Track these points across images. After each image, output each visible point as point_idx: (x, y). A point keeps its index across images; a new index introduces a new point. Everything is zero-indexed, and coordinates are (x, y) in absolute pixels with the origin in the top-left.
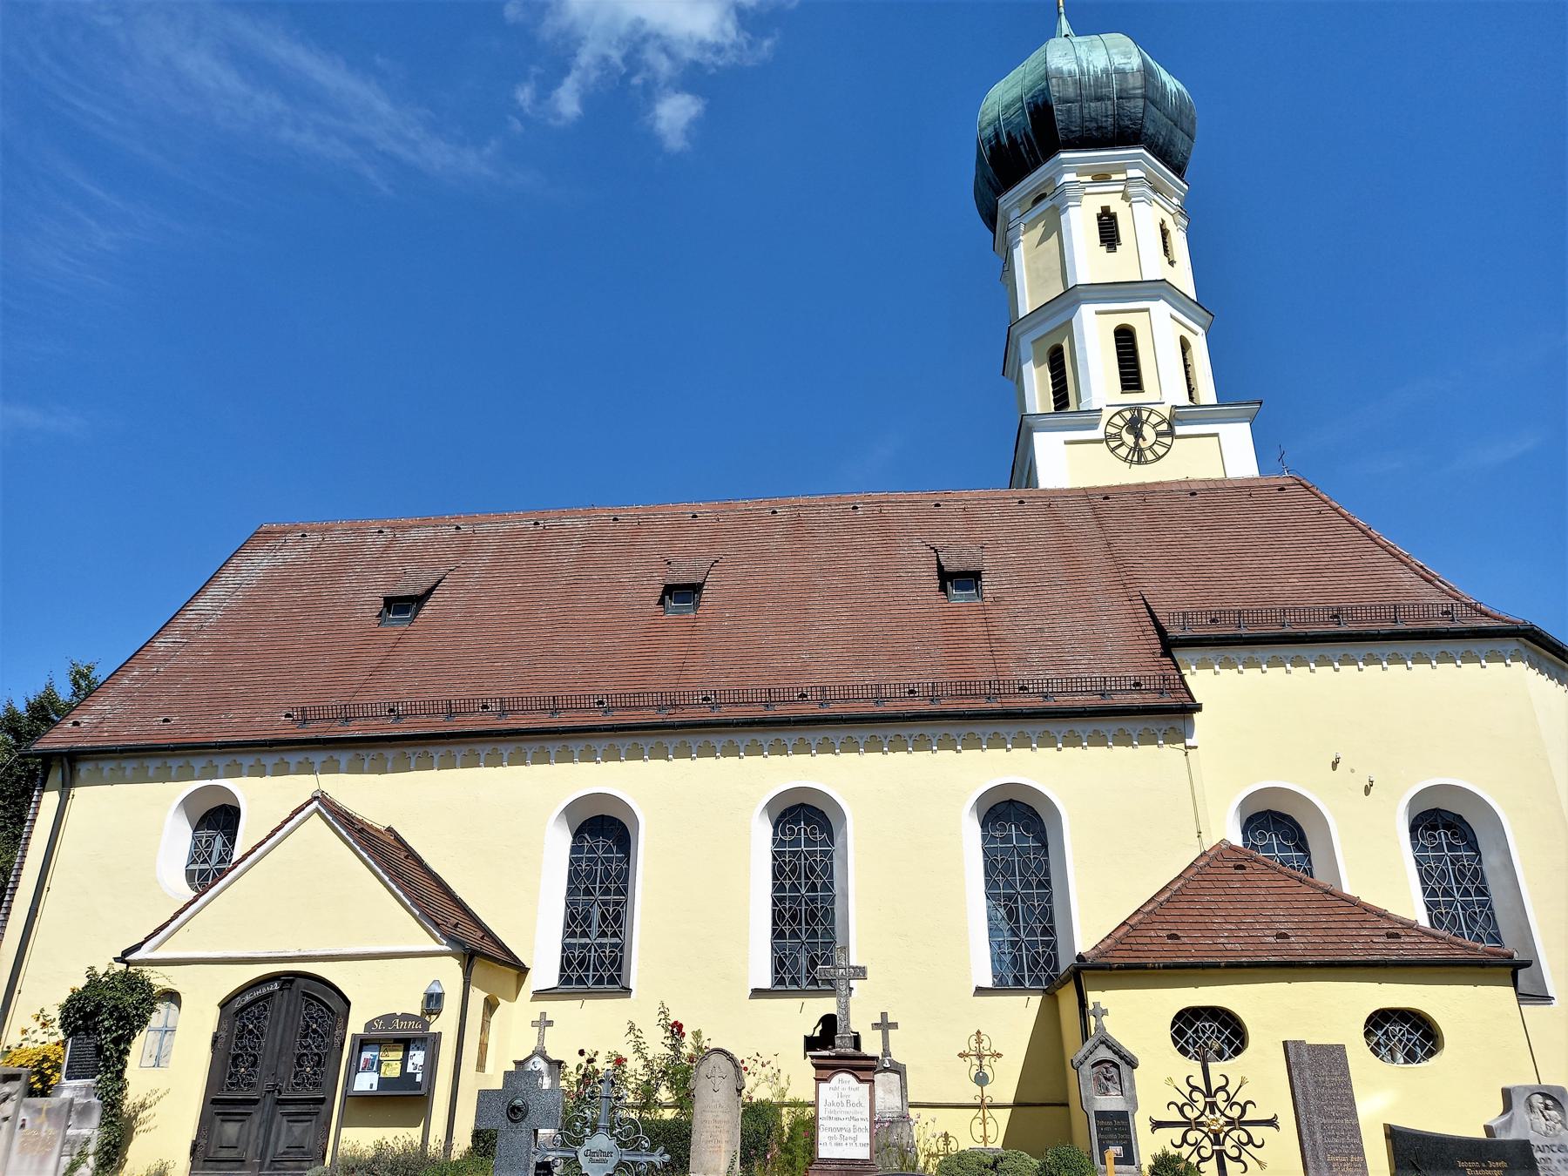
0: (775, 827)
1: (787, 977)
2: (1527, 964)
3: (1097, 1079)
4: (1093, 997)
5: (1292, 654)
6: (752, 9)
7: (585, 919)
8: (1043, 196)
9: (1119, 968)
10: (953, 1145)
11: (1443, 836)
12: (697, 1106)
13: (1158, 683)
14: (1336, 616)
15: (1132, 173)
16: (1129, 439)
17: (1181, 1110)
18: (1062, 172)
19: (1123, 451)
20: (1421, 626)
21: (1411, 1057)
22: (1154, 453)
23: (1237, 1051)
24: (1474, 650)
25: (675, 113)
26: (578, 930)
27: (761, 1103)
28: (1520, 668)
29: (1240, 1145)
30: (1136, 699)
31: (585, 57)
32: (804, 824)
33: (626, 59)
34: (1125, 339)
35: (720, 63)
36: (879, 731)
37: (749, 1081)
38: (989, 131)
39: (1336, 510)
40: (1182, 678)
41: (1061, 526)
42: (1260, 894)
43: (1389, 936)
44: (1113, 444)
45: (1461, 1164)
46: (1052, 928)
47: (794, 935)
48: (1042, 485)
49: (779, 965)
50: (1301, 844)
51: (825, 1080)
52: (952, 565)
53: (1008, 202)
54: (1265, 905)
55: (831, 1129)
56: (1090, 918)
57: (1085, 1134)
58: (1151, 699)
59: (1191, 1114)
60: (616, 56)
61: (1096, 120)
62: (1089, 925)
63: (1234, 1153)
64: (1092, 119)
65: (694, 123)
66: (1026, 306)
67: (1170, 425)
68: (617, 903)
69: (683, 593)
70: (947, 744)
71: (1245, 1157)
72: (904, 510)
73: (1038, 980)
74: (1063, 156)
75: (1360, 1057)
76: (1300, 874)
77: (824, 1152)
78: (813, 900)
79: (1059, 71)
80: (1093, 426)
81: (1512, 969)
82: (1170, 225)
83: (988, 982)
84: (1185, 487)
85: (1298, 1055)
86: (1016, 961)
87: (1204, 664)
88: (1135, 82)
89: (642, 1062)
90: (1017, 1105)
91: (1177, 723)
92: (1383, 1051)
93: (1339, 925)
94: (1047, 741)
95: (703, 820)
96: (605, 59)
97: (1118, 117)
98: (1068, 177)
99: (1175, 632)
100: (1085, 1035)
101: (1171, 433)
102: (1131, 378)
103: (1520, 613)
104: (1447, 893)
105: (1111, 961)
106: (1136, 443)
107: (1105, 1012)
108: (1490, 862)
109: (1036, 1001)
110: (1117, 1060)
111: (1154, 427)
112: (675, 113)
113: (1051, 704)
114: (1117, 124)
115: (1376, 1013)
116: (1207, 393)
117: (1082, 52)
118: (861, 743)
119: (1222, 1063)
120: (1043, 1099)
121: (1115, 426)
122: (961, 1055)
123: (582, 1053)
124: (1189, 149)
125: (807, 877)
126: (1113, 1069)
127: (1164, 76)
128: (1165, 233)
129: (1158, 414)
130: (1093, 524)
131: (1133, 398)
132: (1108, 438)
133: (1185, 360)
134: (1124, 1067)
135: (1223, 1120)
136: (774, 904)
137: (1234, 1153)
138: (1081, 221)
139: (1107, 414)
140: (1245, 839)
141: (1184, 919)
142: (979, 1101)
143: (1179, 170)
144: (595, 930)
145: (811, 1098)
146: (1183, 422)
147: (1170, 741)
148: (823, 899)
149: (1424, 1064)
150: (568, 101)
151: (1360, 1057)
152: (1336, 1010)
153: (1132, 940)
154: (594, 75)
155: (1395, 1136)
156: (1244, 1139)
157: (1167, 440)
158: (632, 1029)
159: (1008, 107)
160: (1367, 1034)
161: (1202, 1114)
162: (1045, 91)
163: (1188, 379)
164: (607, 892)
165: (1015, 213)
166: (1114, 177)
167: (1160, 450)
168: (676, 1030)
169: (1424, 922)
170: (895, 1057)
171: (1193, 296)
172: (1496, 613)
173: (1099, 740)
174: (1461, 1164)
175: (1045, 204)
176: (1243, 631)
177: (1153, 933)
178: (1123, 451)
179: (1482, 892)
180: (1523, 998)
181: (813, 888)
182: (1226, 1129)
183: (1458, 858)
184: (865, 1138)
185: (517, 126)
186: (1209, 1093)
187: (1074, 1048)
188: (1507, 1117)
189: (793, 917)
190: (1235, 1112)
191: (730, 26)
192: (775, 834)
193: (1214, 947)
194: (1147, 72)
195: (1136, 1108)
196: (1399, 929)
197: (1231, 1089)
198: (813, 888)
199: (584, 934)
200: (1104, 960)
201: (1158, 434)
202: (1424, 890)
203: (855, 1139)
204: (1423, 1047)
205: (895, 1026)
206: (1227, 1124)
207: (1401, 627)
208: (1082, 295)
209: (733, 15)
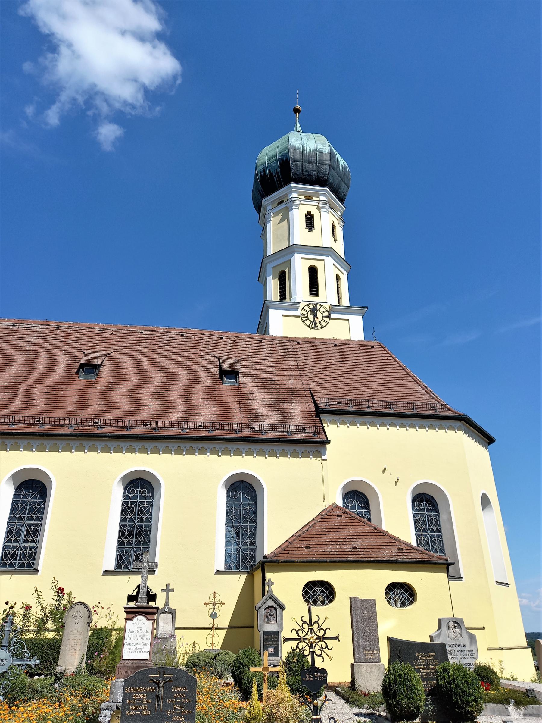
0: (125, 489)
1: (123, 565)
2: (453, 564)
3: (266, 616)
4: (269, 576)
5: (370, 421)
6: (152, 91)
7: (17, 533)
8: (282, 202)
9: (282, 562)
10: (197, 648)
11: (425, 505)
12: (66, 632)
13: (312, 430)
14: (390, 405)
15: (322, 198)
16: (311, 317)
17: (297, 633)
18: (291, 192)
19: (308, 322)
20: (423, 412)
21: (403, 604)
22: (321, 324)
23: (330, 601)
24: (443, 424)
25: (108, 132)
26: (13, 539)
27: (102, 629)
28: (461, 433)
29: (322, 649)
30: (302, 436)
31: (64, 97)
32: (140, 489)
33: (86, 102)
34: (313, 271)
35: (133, 113)
36: (182, 444)
37: (95, 617)
38: (261, 168)
39: (394, 358)
40: (323, 428)
41: (277, 354)
42: (347, 531)
43: (399, 549)
44: (304, 319)
45: (417, 654)
46: (255, 542)
47: (129, 543)
48: (271, 334)
49: (120, 558)
50: (367, 506)
51: (130, 619)
52: (226, 367)
53: (267, 201)
54: (349, 534)
55: (130, 645)
56: (273, 536)
57: (259, 640)
58: (309, 437)
59: (302, 634)
60: (81, 100)
61: (308, 172)
62: (271, 542)
63: (319, 653)
64: (306, 171)
65: (118, 139)
66: (271, 250)
67: (329, 313)
68: (36, 525)
69: (90, 368)
70: (215, 452)
71: (324, 655)
72: (206, 339)
73: (246, 567)
74: (292, 185)
75: (382, 604)
76: (365, 520)
77: (125, 656)
78: (141, 526)
79: (294, 147)
80: (296, 309)
81: (446, 565)
82: (336, 224)
83: (222, 568)
84: (332, 342)
85: (355, 603)
86: (237, 558)
87: (333, 422)
88: (326, 158)
89: (40, 608)
90: (230, 627)
91: (319, 448)
92: (392, 601)
93: (379, 544)
94: (261, 453)
95: (86, 485)
96: (75, 100)
97: (318, 172)
98: (294, 195)
99: (322, 407)
100: (264, 594)
101: (329, 317)
102: (314, 290)
103: (463, 411)
104: (425, 530)
105: (279, 559)
106: (314, 319)
107: (273, 583)
108: (443, 517)
109: (244, 577)
110: (276, 606)
111: (322, 313)
112: (108, 132)
113: (264, 436)
114: (317, 175)
115: (390, 584)
116: (346, 301)
117: (305, 140)
118: (173, 449)
119: (323, 607)
120: (242, 625)
121: (305, 310)
122: (205, 604)
123: (7, 603)
124: (347, 192)
125: (139, 515)
126: (274, 611)
127: (339, 157)
128: (334, 227)
129: (324, 308)
130: (292, 354)
131: (314, 299)
132: (302, 316)
133: (338, 285)
134: (279, 610)
135: (315, 637)
136: (120, 528)
137: (319, 653)
138: (298, 217)
139: (302, 304)
140: (344, 503)
141: (313, 539)
142: (211, 626)
143: (342, 200)
144: (22, 538)
145: (123, 626)
146: (335, 312)
147: (316, 456)
148: (146, 526)
149: (408, 607)
150: (53, 117)
151: (382, 604)
152: (371, 583)
153: (289, 549)
154: (68, 106)
155: (390, 640)
156: (324, 646)
157: (327, 320)
158: (36, 591)
159: (270, 158)
160: (386, 594)
161: (307, 634)
162: (287, 154)
163: (338, 294)
164: (31, 519)
165: (269, 208)
166: (314, 199)
167: (324, 324)
168: (60, 591)
169: (414, 543)
170: (170, 606)
171: (344, 257)
172: (453, 409)
173: (284, 454)
174: (417, 654)
175: (283, 206)
176: (351, 409)
177: (299, 546)
178: (308, 322)
179: (439, 530)
180: (451, 577)
181: (141, 520)
182: (316, 641)
183: (430, 515)
184: (147, 648)
185: (25, 125)
186: (310, 624)
187: (259, 600)
188: (439, 632)
189: (129, 535)
190: (321, 633)
191: (140, 96)
192: (125, 492)
193: (325, 553)
194: (332, 155)
195: (282, 629)
196: (403, 546)
197: (320, 622)
198: (141, 520)
199: (16, 541)
200: (276, 558)
201: (324, 317)
202: (416, 529)
203: (142, 649)
204: (408, 599)
205: (173, 590)
206: (317, 639)
207: (415, 412)
208: (296, 249)
209: (142, 90)
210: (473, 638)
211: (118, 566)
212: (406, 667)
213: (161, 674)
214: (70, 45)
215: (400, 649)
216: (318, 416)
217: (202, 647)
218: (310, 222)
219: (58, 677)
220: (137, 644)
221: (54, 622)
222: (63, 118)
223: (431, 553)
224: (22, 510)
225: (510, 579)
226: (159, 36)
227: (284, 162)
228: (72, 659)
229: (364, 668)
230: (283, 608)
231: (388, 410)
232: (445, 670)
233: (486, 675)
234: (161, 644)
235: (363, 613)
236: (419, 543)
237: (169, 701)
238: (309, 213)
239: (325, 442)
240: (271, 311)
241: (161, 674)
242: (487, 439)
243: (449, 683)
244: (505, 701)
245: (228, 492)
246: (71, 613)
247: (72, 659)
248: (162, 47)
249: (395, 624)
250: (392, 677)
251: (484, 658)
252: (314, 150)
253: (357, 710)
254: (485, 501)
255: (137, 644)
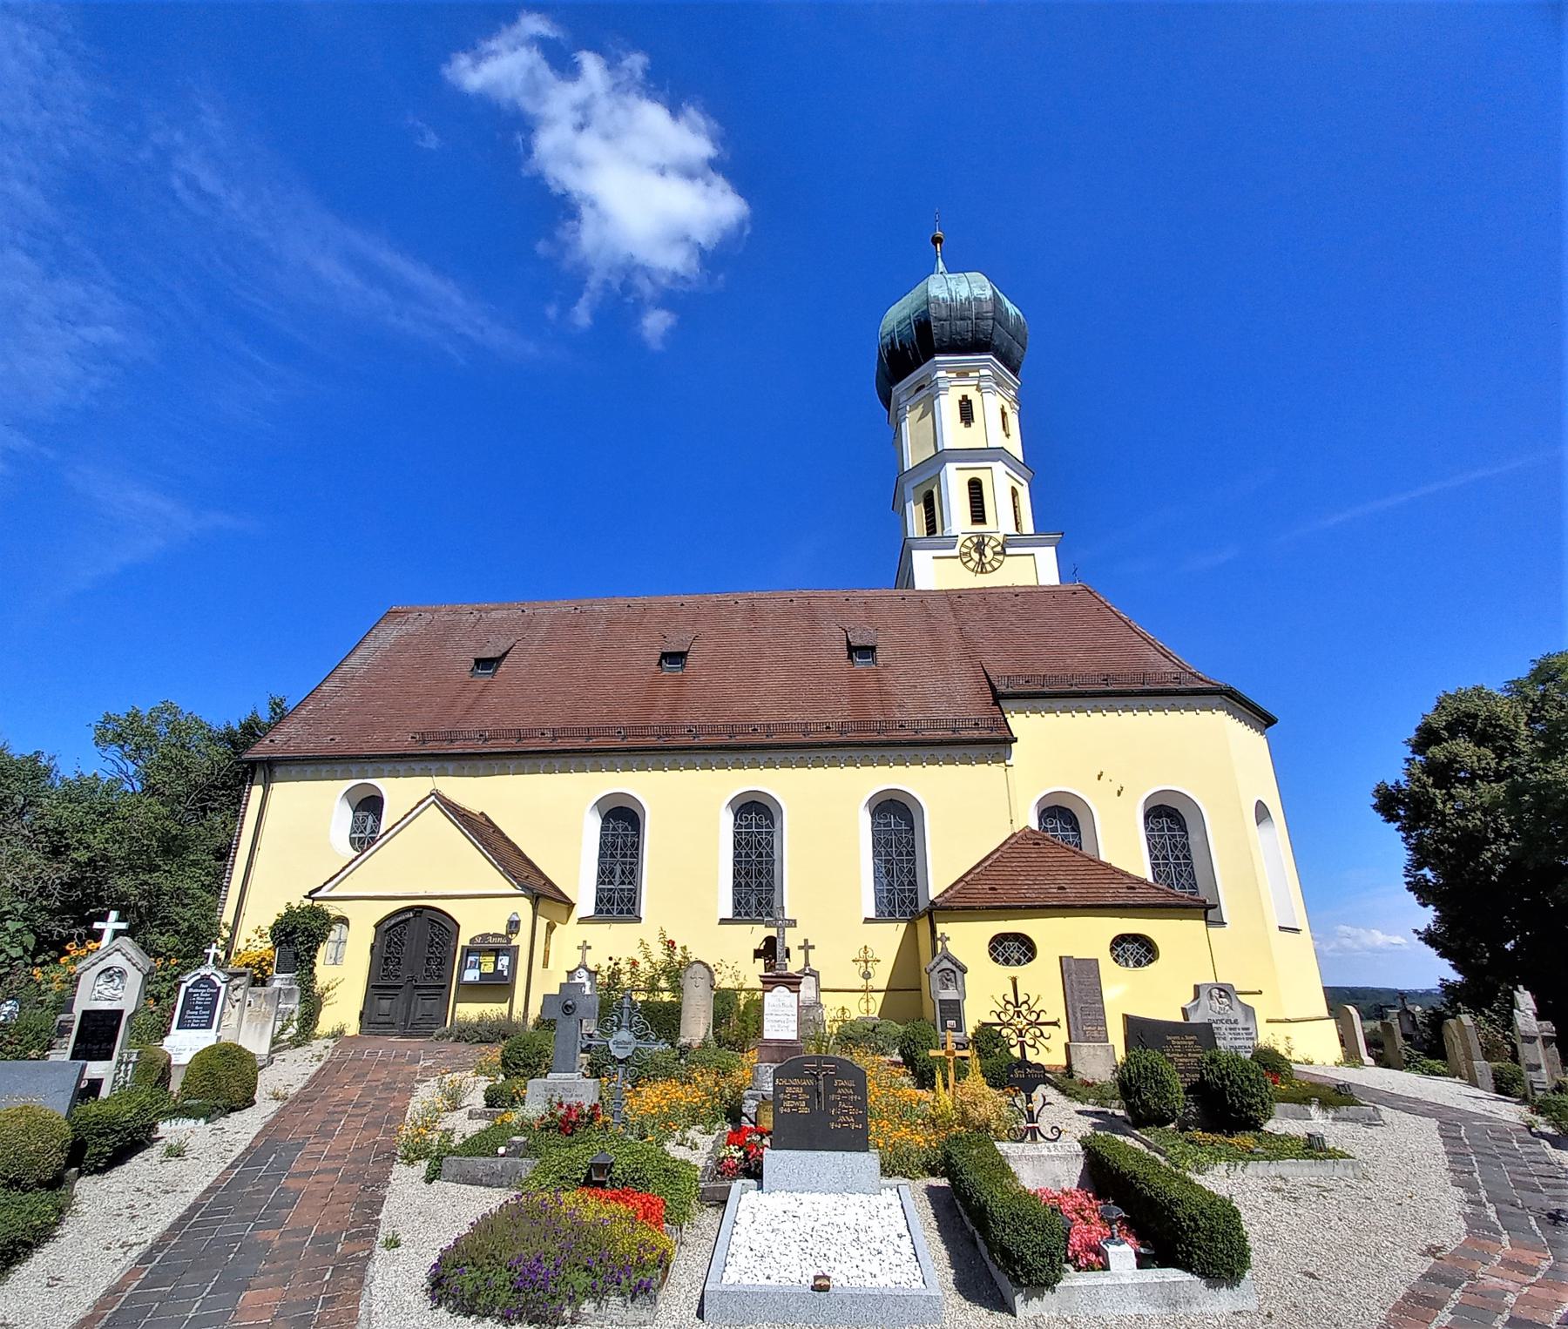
15: (983, 372)
16: (976, 556)
21: (1138, 964)
25: (656, 323)
28: (1221, 714)
29: (1035, 1037)
30: (975, 734)
31: (593, 283)
32: (756, 817)
33: (622, 286)
34: (975, 487)
37: (717, 978)
41: (930, 616)
42: (1048, 863)
49: (737, 903)
50: (1076, 828)
52: (856, 642)
53: (898, 389)
58: (985, 734)
59: (1005, 1018)
63: (1031, 1042)
65: (671, 330)
66: (910, 462)
69: (675, 658)
72: (825, 603)
76: (1072, 847)
78: (760, 863)
81: (1205, 910)
82: (1008, 410)
88: (988, 307)
90: (888, 990)
95: (689, 812)
97: (975, 332)
98: (941, 374)
99: (1002, 689)
101: (1003, 553)
102: (978, 515)
104: (1165, 858)
108: (1194, 838)
109: (903, 926)
112: (656, 323)
116: (1028, 527)
117: (952, 285)
120: (907, 986)
127: (1008, 304)
128: (1004, 414)
131: (979, 528)
134: (958, 973)
143: (1014, 371)
150: (582, 315)
152: (1090, 936)
160: (1112, 949)
164: (625, 856)
167: (996, 565)
168: (671, 944)
169: (1151, 880)
175: (924, 392)
180: (1209, 923)
184: (795, 1027)
189: (747, 874)
190: (1033, 1017)
191: (694, 263)
194: (996, 300)
197: (1031, 1003)
198: (760, 855)
199: (611, 883)
201: (995, 553)
210: (1249, 1011)
211: (737, 913)
212: (1153, 1055)
213: (819, 1064)
214: (593, 205)
215: (1138, 1030)
216: (996, 703)
217: (854, 1014)
218: (966, 412)
219: (684, 1051)
220: (780, 1018)
221: (668, 978)
222: (595, 315)
223: (1177, 890)
224: (613, 845)
225: (1301, 921)
226: (714, 165)
227: (923, 325)
228: (696, 1027)
229: (1084, 1050)
230: (964, 971)
231: (1104, 688)
232: (1213, 1061)
233: (1271, 1063)
234: (808, 1015)
235: (1080, 979)
236: (1157, 876)
237: (833, 1097)
238: (965, 397)
239: (1010, 740)
240: (914, 553)
241: (819, 1064)
242: (1262, 720)
243: (1222, 1079)
244: (1306, 1101)
245: (873, 815)
246: (689, 974)
247: (696, 1027)
248: (719, 182)
249: (1130, 994)
250: (1134, 1069)
251: (1267, 1036)
252: (967, 299)
253: (1079, 1107)
254: (1262, 813)
255: (780, 1018)
